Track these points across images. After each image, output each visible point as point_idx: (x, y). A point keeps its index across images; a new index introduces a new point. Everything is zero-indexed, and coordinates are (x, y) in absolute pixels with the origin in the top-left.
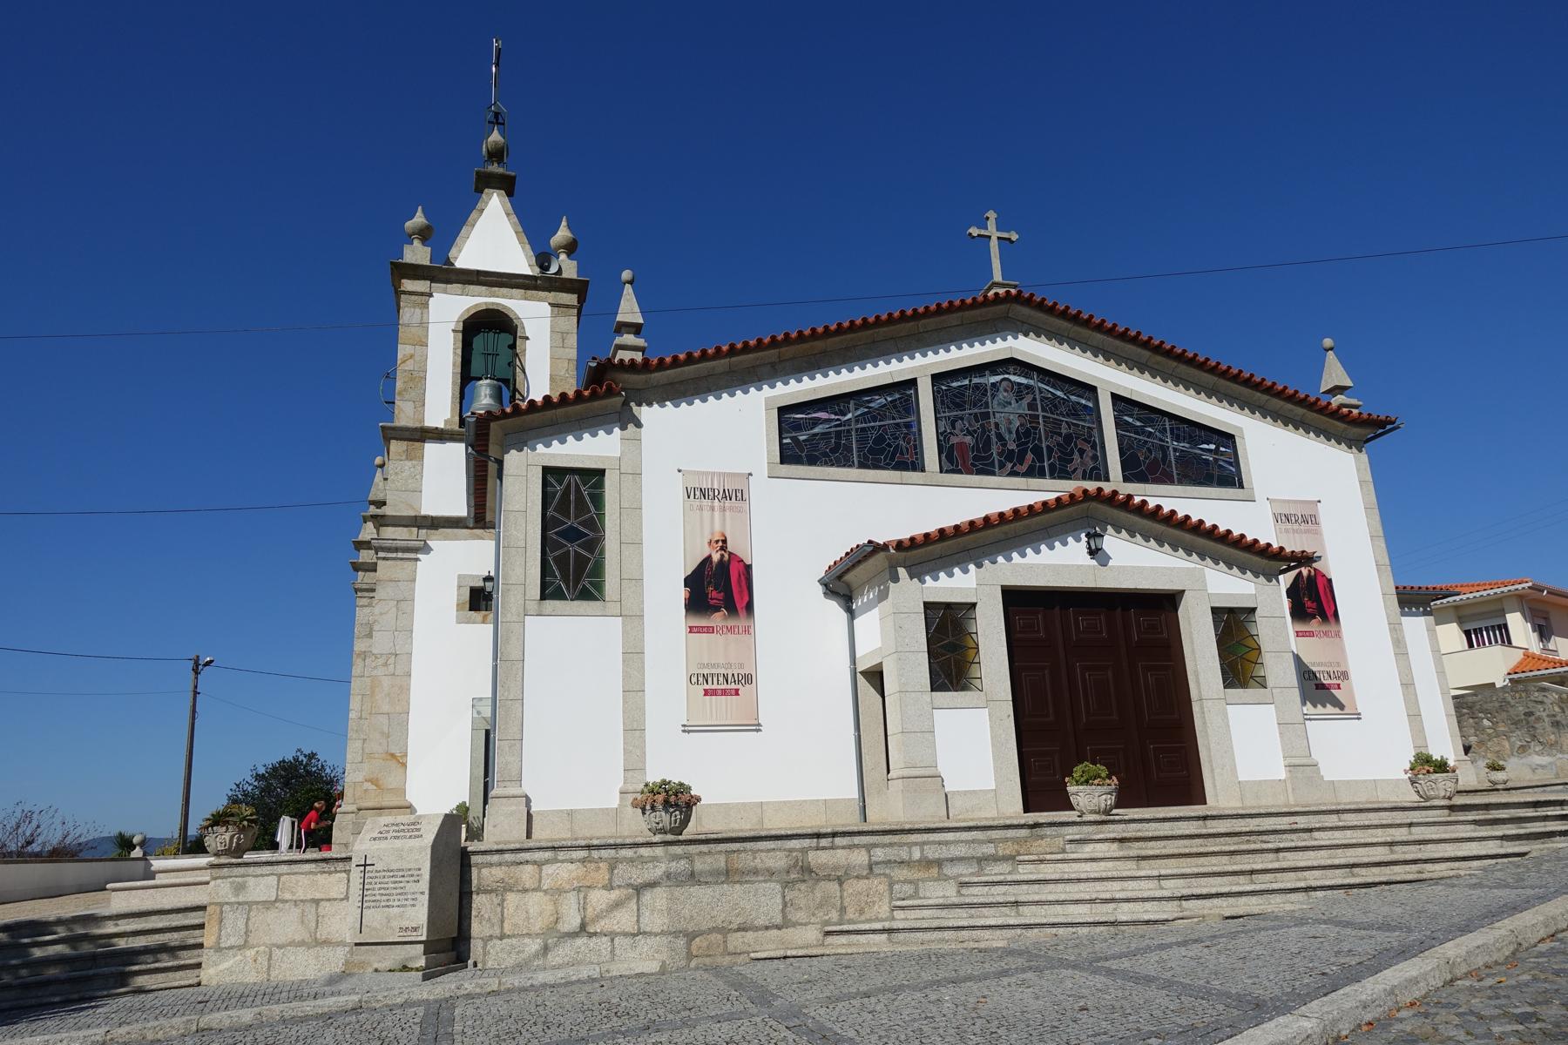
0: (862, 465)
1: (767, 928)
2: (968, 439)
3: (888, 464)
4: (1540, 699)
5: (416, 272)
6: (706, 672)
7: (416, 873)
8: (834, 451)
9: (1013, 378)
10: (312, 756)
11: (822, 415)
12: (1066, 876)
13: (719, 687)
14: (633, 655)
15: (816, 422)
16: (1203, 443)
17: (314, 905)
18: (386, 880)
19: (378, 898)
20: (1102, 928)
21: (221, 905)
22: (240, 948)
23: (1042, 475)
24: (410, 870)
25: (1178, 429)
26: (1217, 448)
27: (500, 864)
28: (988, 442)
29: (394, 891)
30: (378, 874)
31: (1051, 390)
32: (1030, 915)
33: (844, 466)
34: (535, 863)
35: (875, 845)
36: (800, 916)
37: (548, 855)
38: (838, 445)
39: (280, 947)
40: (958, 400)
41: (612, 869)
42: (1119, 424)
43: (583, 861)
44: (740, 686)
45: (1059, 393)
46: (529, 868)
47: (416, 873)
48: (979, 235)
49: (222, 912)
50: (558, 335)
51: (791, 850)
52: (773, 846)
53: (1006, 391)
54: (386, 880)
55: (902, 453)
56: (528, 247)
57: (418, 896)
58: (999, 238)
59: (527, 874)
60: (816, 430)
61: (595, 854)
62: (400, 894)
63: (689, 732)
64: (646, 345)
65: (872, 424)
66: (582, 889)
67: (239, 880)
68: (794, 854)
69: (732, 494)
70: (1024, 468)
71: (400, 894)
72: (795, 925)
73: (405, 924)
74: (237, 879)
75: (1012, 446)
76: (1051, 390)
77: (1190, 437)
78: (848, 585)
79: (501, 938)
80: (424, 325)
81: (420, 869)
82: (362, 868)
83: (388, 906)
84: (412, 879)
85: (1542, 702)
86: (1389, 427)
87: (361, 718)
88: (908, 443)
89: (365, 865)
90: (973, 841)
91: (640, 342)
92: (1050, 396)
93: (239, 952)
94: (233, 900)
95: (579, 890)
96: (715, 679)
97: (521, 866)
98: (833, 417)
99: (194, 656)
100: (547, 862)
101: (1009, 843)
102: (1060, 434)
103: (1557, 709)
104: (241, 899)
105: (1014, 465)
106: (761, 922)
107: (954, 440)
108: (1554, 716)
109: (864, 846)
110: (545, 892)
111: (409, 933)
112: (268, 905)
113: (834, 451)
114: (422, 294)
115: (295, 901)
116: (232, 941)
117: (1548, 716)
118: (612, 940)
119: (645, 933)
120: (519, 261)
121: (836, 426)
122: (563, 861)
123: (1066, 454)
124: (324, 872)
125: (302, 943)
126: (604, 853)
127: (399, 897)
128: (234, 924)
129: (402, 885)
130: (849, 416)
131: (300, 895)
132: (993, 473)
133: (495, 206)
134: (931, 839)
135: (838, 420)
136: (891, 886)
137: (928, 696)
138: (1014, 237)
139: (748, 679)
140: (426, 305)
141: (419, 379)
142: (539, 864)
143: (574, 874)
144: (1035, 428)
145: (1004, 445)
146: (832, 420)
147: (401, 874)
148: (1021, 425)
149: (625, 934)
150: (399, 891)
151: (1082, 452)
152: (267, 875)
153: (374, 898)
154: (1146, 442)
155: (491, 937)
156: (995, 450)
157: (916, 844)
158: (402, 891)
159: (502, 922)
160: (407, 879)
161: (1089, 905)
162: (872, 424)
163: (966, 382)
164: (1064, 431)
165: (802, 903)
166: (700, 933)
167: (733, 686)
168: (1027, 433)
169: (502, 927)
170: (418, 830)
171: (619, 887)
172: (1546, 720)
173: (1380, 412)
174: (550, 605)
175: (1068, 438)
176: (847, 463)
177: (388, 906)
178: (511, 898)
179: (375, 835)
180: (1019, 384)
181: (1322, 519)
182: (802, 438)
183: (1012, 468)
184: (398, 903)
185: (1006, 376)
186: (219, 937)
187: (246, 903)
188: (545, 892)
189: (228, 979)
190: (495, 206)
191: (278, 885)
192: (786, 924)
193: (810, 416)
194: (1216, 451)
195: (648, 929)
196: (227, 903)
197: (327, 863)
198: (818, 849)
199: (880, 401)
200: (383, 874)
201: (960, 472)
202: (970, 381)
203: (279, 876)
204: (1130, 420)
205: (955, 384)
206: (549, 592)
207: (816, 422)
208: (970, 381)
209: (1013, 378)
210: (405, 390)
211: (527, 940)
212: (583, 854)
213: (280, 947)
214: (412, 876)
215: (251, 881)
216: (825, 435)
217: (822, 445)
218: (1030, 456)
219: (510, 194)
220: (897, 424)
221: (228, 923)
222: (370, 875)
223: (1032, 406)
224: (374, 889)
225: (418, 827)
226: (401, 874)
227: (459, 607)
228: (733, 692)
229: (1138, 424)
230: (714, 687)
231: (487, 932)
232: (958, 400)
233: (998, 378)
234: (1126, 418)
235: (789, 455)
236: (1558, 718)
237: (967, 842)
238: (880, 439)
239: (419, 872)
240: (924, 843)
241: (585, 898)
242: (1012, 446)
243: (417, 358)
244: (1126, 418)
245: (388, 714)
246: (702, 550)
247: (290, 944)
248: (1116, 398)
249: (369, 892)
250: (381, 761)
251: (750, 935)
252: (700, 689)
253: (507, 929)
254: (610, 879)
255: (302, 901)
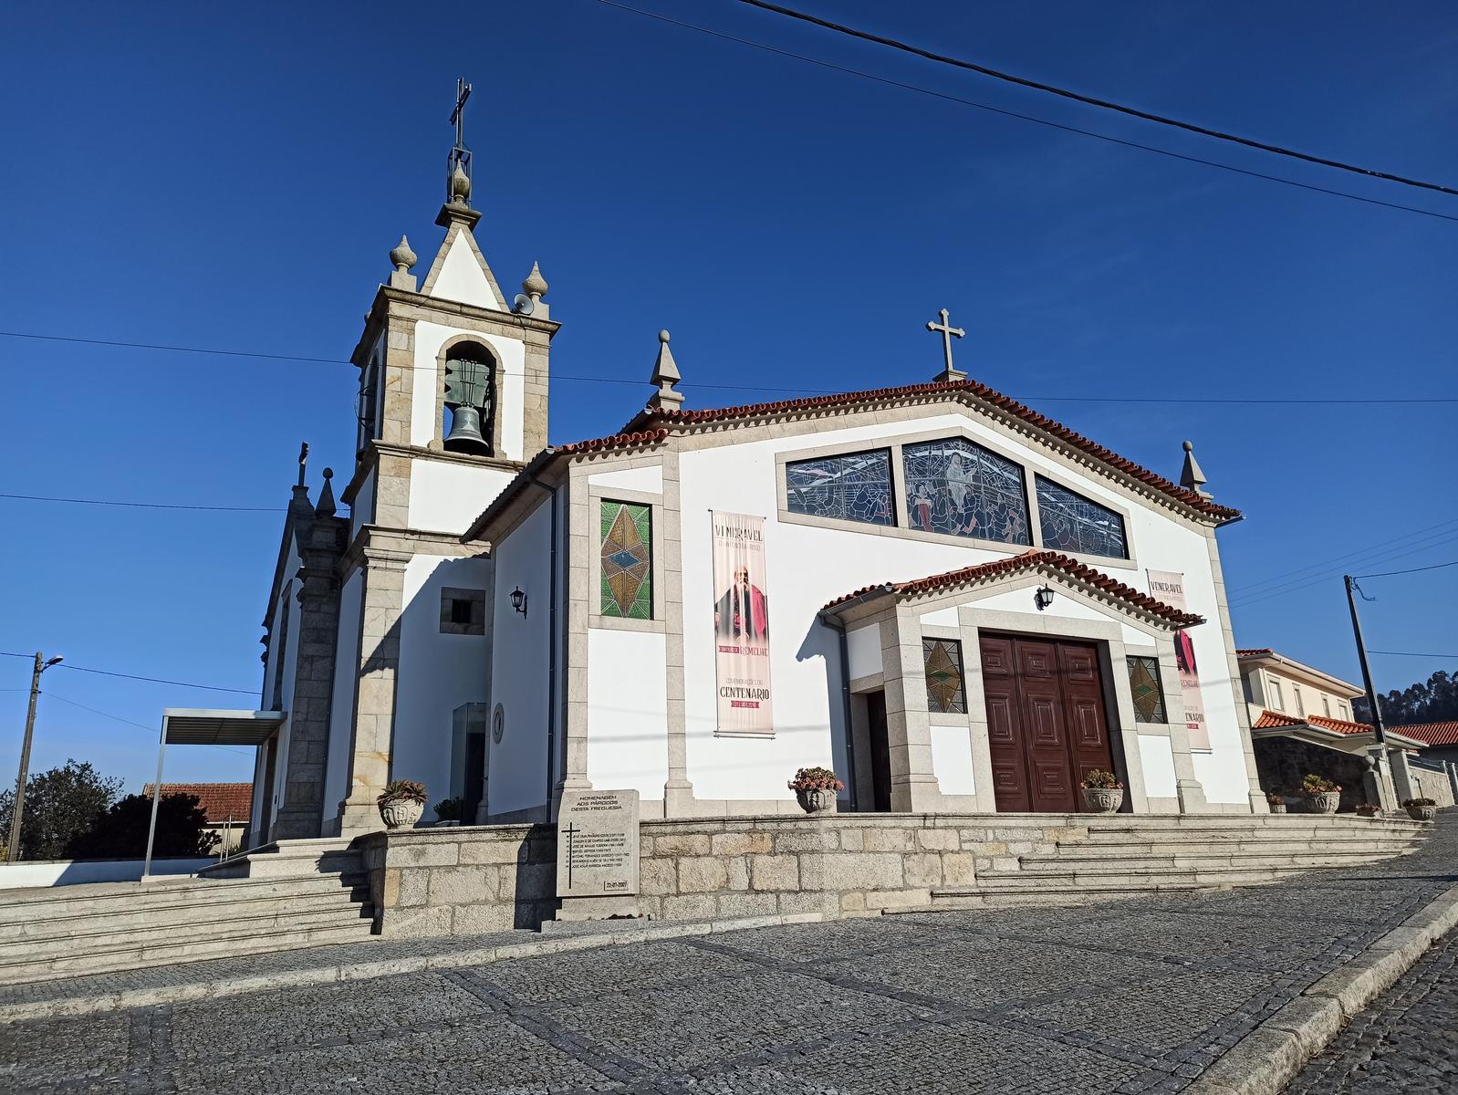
0: (850, 518)
1: (893, 890)
2: (928, 502)
3: (869, 518)
4: (1292, 749)
5: (405, 298)
6: (733, 686)
7: (619, 838)
8: (828, 503)
9: (962, 453)
10: (86, 767)
11: (819, 472)
12: (1105, 857)
13: (743, 700)
14: (675, 667)
15: (814, 477)
16: (1100, 520)
17: (496, 869)
18: (592, 843)
19: (585, 858)
20: (1146, 894)
21: (401, 869)
22: (422, 906)
23: (983, 536)
24: (614, 835)
25: (1082, 506)
26: (1110, 524)
27: (673, 834)
28: (943, 505)
29: (600, 853)
30: (583, 839)
31: (990, 466)
32: (1082, 882)
33: (835, 517)
34: (706, 833)
35: (963, 827)
36: (912, 881)
37: (717, 826)
38: (831, 498)
39: (463, 905)
40: (921, 468)
41: (774, 839)
42: (1041, 499)
43: (748, 832)
44: (759, 700)
45: (996, 469)
46: (701, 837)
47: (619, 838)
48: (935, 329)
49: (401, 876)
50: (530, 374)
51: (906, 828)
52: (894, 825)
53: (956, 463)
54: (592, 843)
55: (879, 510)
56: (495, 284)
57: (623, 857)
58: (950, 333)
59: (699, 842)
60: (814, 484)
61: (759, 826)
62: (606, 855)
63: (718, 736)
64: (683, 398)
65: (857, 483)
66: (749, 856)
67: (419, 847)
68: (908, 831)
69: (743, 533)
70: (969, 530)
71: (606, 855)
72: (912, 888)
73: (611, 880)
74: (416, 846)
75: (961, 510)
76: (990, 466)
77: (1091, 514)
78: (842, 620)
79: (677, 895)
80: (410, 351)
81: (623, 835)
82: (568, 834)
83: (595, 866)
84: (617, 843)
85: (1294, 752)
86: (1232, 518)
87: (306, 720)
88: (884, 502)
89: (571, 831)
90: (1028, 828)
91: (678, 395)
92: (988, 470)
93: (421, 910)
94: (413, 865)
95: (745, 855)
96: (740, 693)
97: (693, 836)
98: (827, 474)
99: (34, 655)
100: (716, 832)
101: (1053, 831)
102: (996, 504)
103: (1305, 758)
104: (421, 863)
105: (963, 526)
106: (890, 884)
107: (918, 502)
108: (1303, 764)
109: (955, 827)
110: (716, 857)
111: (617, 888)
112: (450, 869)
113: (828, 503)
114: (408, 320)
115: (477, 865)
116: (413, 901)
117: (1298, 764)
118: (778, 897)
119: (806, 891)
120: (486, 295)
121: (829, 482)
122: (729, 832)
123: (1000, 520)
124: (505, 840)
125: (486, 902)
126: (767, 826)
127: (604, 858)
128: (415, 884)
129: (607, 848)
130: (839, 474)
131: (482, 859)
132: (946, 532)
133: (461, 242)
134: (1000, 824)
135: (831, 477)
136: (974, 859)
137: (926, 715)
138: (962, 333)
139: (765, 694)
140: (412, 332)
141: (406, 398)
142: (710, 834)
143: (741, 842)
144: (978, 497)
145: (955, 509)
146: (825, 477)
147: (606, 838)
148: (968, 493)
149: (789, 892)
150: (604, 853)
151: (1012, 519)
152: (447, 843)
153: (580, 859)
154: (1059, 515)
155: (668, 895)
156: (949, 511)
157: (990, 828)
158: (607, 853)
159: (677, 882)
160: (611, 843)
161: (1128, 878)
162: (857, 483)
163: (927, 453)
164: (999, 501)
165: (916, 870)
166: (847, 891)
167: (754, 700)
168: (972, 500)
169: (678, 886)
170: (616, 802)
171: (782, 853)
172: (1296, 767)
173: (1229, 506)
174: (609, 620)
175: (1002, 507)
176: (835, 514)
177: (595, 866)
178: (685, 862)
179: (575, 806)
180: (966, 459)
181: (1184, 589)
182: (803, 490)
183: (961, 529)
184: (605, 863)
185: (957, 451)
186: (400, 897)
187: (427, 867)
188: (716, 857)
189: (410, 935)
190: (461, 242)
191: (459, 852)
192: (905, 887)
193: (809, 472)
194: (1109, 527)
195: (809, 887)
196: (407, 868)
197: (508, 833)
198: (924, 828)
199: (861, 464)
200: (589, 838)
201: (922, 529)
202: (930, 453)
203: (459, 843)
204: (1047, 496)
205: (918, 455)
206: (609, 612)
207: (814, 477)
208: (930, 453)
209: (962, 453)
210: (393, 410)
211: (701, 897)
212: (748, 826)
213: (463, 905)
214: (617, 840)
215: (431, 848)
216: (821, 489)
217: (818, 498)
218: (974, 521)
219: (471, 228)
220: (876, 485)
221: (410, 887)
222: (576, 839)
223: (975, 478)
224: (581, 851)
225: (614, 800)
226: (606, 838)
227: (443, 618)
228: (754, 705)
229: (1053, 500)
230: (739, 699)
231: (664, 890)
232: (921, 468)
233: (950, 452)
234: (1044, 494)
235: (793, 507)
236: (1306, 765)
237: (1024, 828)
238: (862, 497)
239: (622, 837)
240: (996, 827)
241: (752, 862)
242: (961, 510)
243: (404, 380)
244: (1044, 494)
245: (376, 715)
246: (726, 582)
247: (474, 902)
248: (1037, 476)
249: (577, 854)
250: (370, 759)
251: (881, 895)
252: (728, 700)
253: (683, 888)
254: (774, 847)
255: (484, 865)
